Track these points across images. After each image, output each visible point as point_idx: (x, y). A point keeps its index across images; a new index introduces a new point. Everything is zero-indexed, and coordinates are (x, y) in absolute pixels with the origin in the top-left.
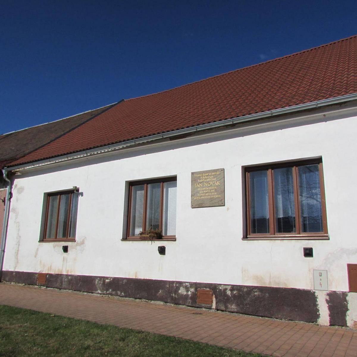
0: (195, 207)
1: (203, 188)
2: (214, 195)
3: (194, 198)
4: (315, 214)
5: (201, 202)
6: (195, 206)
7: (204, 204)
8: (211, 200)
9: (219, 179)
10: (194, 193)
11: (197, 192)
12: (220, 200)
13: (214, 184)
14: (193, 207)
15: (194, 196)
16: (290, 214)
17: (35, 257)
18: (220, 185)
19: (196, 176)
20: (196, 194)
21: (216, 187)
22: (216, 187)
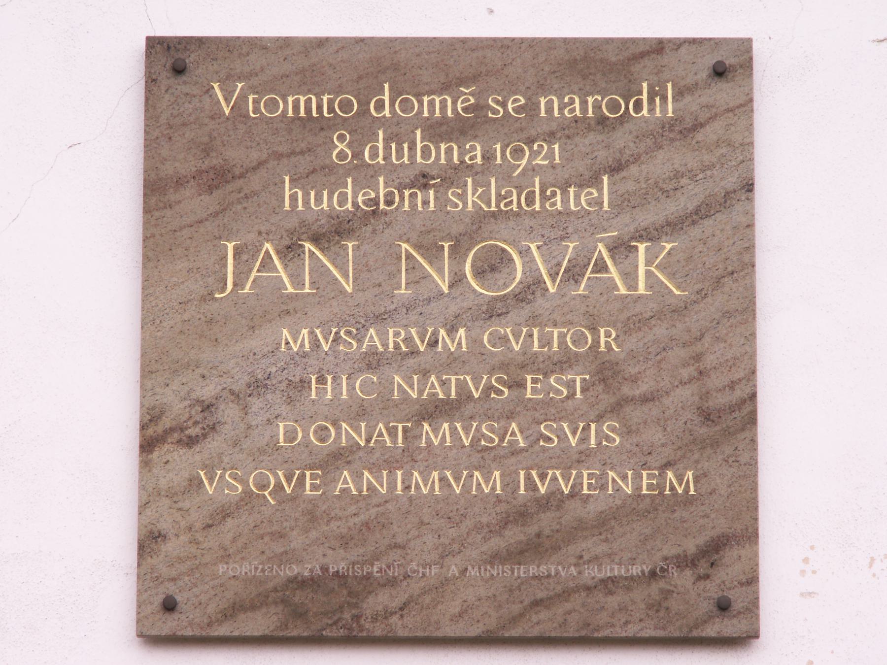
0: (223, 630)
1: (381, 319)
2: (583, 457)
3: (195, 484)
4: (490, 553)
5: (338, 563)
6: (231, 612)
7: (381, 600)
8: (514, 535)
9: (672, 208)
10: (207, 391)
11: (258, 386)
12: (691, 546)
13: (574, 274)
14: (169, 625)
15: (191, 442)
16: (716, 597)
17: (802, 595)
18: (680, 310)
19: (239, 109)
20: (229, 412)
21: (606, 337)
22: (606, 337)
